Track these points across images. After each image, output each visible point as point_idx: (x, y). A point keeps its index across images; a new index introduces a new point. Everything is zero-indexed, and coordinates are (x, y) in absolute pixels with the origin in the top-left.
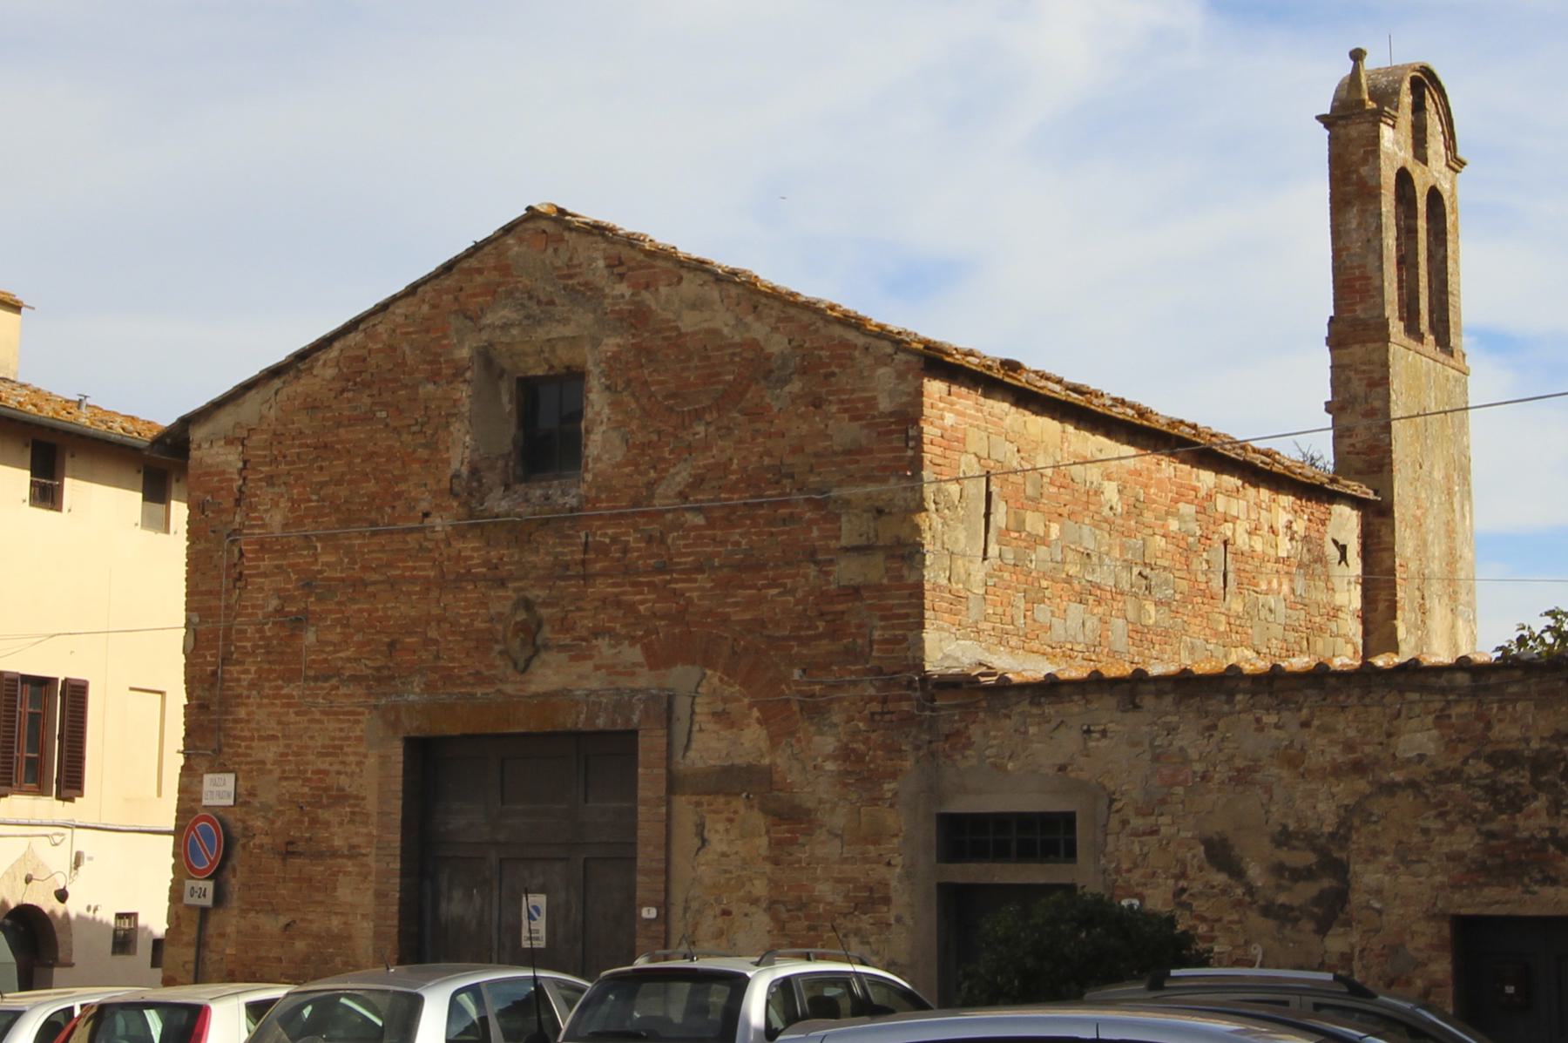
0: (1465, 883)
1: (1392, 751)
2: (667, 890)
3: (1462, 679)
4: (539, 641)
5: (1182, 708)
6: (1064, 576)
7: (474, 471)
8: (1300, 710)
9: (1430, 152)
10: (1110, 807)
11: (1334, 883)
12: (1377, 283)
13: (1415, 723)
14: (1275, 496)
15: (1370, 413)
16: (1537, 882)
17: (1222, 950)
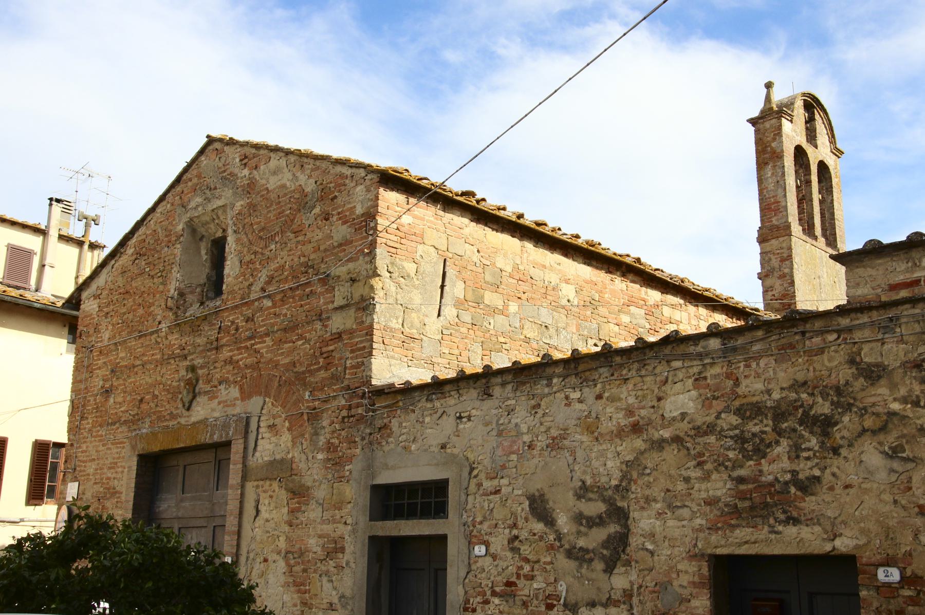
0: (719, 525)
1: (661, 412)
2: (238, 546)
3: (714, 344)
4: (197, 390)
5: (518, 394)
6: (523, 337)
7: (181, 294)
8: (595, 385)
9: (819, 142)
10: (470, 473)
11: (618, 528)
12: (783, 204)
13: (679, 386)
14: (712, 314)
15: (782, 277)
16: (780, 522)
17: (539, 587)
